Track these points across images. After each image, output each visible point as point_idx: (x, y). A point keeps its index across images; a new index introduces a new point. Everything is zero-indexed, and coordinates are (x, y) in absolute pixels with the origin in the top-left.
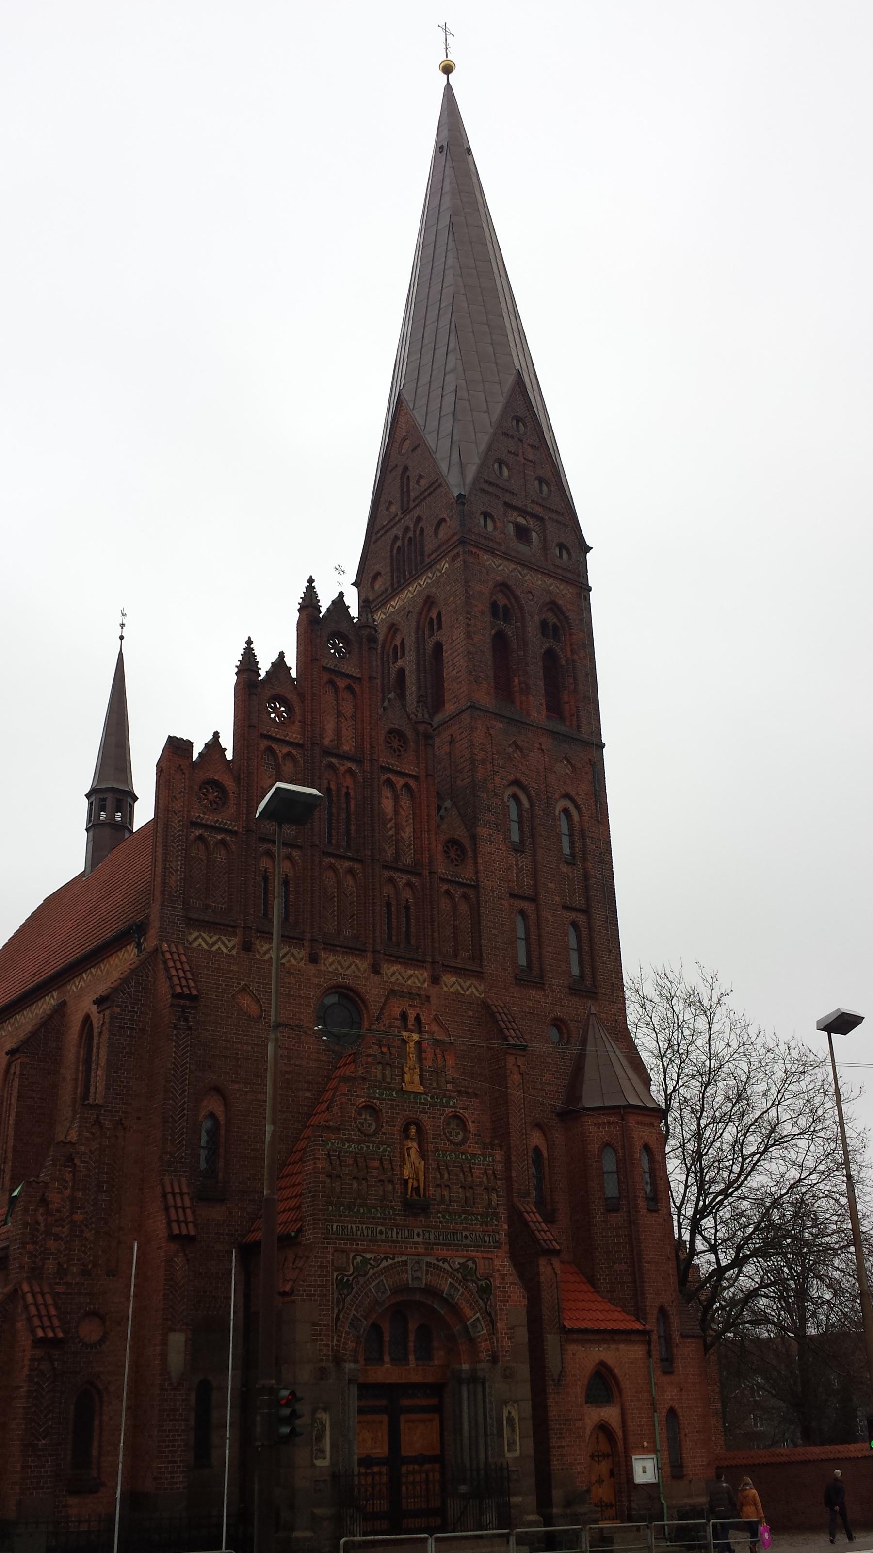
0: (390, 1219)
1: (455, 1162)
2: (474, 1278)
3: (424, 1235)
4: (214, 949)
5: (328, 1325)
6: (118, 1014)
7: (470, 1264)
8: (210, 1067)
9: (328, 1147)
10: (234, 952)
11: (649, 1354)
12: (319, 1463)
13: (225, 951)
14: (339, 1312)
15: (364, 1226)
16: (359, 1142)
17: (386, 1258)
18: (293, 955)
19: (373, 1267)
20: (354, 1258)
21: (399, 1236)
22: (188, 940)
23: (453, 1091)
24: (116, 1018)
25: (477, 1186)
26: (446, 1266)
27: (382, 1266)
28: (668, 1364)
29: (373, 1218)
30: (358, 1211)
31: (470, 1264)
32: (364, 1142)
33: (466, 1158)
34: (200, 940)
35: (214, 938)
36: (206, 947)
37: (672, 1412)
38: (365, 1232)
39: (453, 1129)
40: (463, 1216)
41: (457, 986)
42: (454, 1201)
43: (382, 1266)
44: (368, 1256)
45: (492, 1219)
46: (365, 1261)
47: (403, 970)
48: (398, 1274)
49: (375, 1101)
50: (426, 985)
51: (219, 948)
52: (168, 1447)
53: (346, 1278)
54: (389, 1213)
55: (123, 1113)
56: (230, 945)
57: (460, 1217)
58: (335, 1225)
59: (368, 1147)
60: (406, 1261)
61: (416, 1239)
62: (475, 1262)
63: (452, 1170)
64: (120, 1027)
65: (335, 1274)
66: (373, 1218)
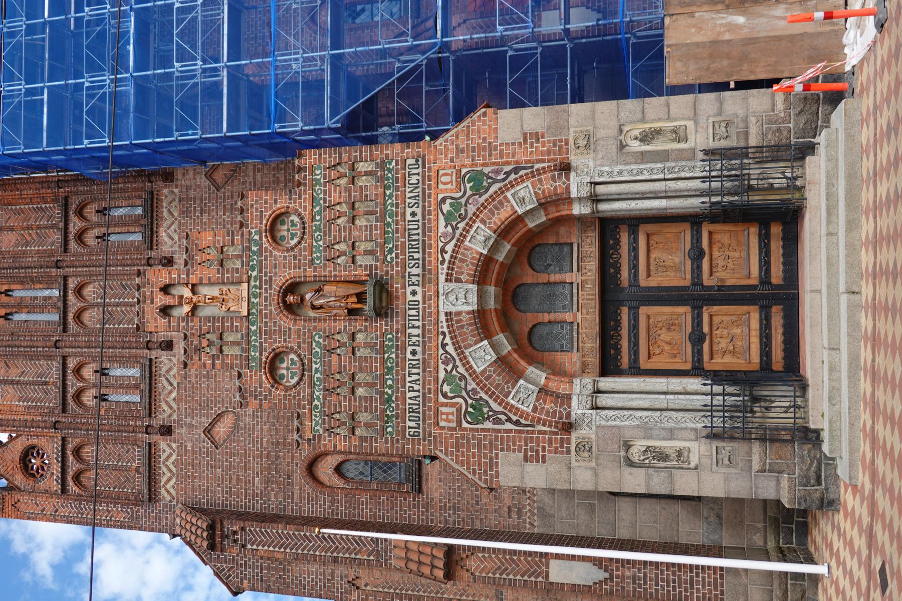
0: (397, 338)
1: (325, 235)
2: (463, 201)
3: (413, 284)
4: (174, 470)
5: (526, 439)
6: (249, 582)
8: (289, 477)
9: (321, 431)
10: (174, 445)
13: (174, 457)
14: (509, 420)
15: (408, 379)
16: (312, 385)
17: (444, 346)
18: (168, 371)
19: (455, 367)
20: (445, 396)
21: (417, 323)
22: (171, 501)
23: (242, 235)
24: (253, 584)
25: (350, 195)
26: (449, 248)
27: (454, 354)
29: (397, 365)
30: (390, 387)
31: (446, 207)
32: (311, 377)
33: (319, 213)
34: (168, 487)
35: (164, 469)
36: (174, 480)
38: (415, 377)
39: (288, 230)
40: (389, 220)
42: (371, 235)
43: (454, 354)
44: (442, 375)
45: (390, 170)
46: (448, 379)
47: (165, 224)
48: (462, 327)
49: (264, 360)
50: (176, 191)
51: (173, 463)
52: (674, 587)
53: (470, 409)
54: (390, 340)
55: (342, 580)
56: (168, 451)
57: (389, 225)
58: (409, 424)
59: (317, 370)
60: (446, 314)
61: (419, 297)
62: (444, 200)
63: (335, 237)
64: (261, 581)
65: (465, 425)
66: (397, 365)
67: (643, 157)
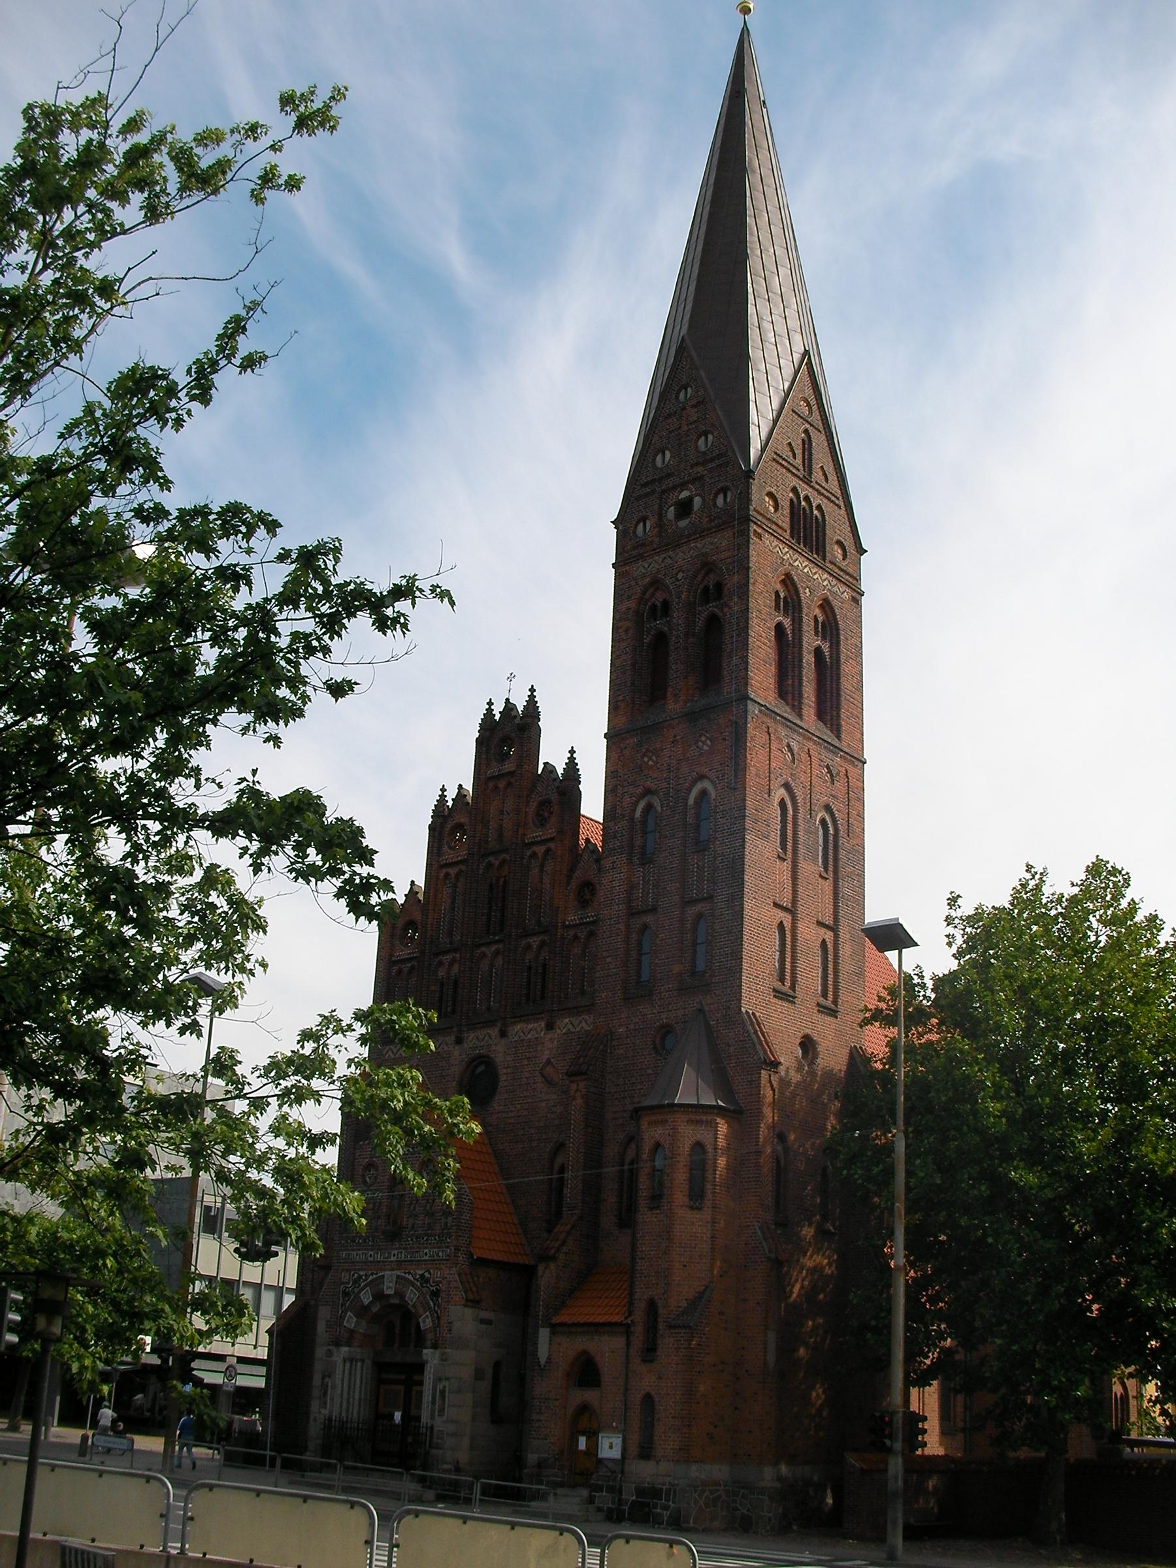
7: (427, 1275)
11: (628, 1344)
12: (323, 1411)
28: (650, 1351)
37: (648, 1399)
41: (570, 1026)
46: (360, 1277)
61: (392, 1259)
67: (434, 1389)
